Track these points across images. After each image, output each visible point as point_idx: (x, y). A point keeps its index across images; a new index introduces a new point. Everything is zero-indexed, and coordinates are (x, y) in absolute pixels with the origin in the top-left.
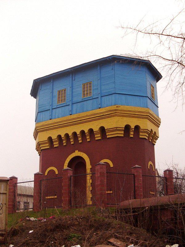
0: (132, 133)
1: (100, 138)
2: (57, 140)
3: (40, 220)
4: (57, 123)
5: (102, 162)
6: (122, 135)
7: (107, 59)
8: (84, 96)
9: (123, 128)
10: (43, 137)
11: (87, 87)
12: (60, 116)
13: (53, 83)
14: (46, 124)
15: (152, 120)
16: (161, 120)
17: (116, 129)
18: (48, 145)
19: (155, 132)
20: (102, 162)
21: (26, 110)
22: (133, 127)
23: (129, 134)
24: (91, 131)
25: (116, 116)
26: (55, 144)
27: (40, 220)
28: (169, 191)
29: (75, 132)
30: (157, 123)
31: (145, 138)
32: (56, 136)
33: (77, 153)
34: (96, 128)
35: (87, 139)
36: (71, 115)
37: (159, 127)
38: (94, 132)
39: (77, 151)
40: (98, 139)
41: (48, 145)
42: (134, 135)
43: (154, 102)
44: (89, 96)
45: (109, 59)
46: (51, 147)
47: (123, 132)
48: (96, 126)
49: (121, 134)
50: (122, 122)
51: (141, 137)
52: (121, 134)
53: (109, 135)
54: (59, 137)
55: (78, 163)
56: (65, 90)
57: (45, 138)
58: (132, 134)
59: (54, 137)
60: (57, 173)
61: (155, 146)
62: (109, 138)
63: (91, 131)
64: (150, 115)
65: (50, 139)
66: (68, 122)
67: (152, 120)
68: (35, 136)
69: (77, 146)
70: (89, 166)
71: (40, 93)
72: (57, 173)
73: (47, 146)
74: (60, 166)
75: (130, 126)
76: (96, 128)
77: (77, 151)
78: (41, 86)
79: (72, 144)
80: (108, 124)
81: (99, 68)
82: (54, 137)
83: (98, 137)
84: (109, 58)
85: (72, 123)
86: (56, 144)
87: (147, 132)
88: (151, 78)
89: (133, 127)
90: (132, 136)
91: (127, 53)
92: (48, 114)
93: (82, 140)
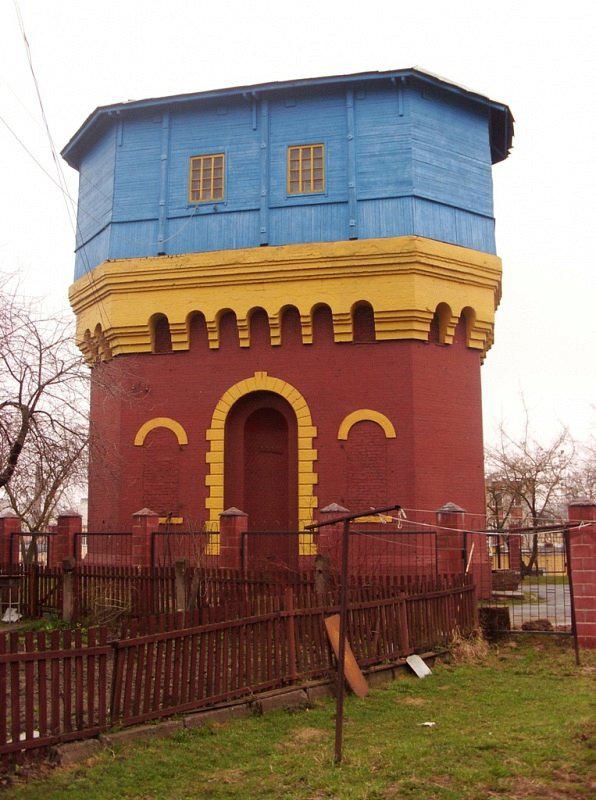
0: (451, 332)
1: (185, 347)
2: (184, 327)
6: (425, 337)
7: (106, 114)
8: (195, 194)
10: (132, 312)
11: (208, 173)
13: (170, 127)
14: (296, 256)
17: (408, 317)
19: (467, 313)
22: (305, 310)
24: (322, 311)
25: (109, 293)
26: (243, 339)
30: (500, 273)
31: (120, 355)
34: (341, 305)
36: (356, 239)
38: (373, 313)
41: (148, 340)
44: (311, 190)
45: (249, 94)
46: (155, 349)
47: (427, 328)
48: (340, 299)
51: (337, 339)
52: (146, 345)
53: (383, 332)
54: (196, 319)
55: (262, 419)
59: (177, 316)
62: (275, 346)
63: (322, 311)
65: (160, 323)
69: (260, 357)
70: (306, 431)
71: (106, 159)
74: (198, 425)
76: (341, 305)
78: (269, 124)
79: (211, 347)
80: (384, 296)
81: (350, 103)
82: (177, 316)
83: (344, 333)
84: (114, 109)
85: (198, 281)
86: (180, 342)
91: (424, 67)
92: (147, 234)
93: (221, 340)
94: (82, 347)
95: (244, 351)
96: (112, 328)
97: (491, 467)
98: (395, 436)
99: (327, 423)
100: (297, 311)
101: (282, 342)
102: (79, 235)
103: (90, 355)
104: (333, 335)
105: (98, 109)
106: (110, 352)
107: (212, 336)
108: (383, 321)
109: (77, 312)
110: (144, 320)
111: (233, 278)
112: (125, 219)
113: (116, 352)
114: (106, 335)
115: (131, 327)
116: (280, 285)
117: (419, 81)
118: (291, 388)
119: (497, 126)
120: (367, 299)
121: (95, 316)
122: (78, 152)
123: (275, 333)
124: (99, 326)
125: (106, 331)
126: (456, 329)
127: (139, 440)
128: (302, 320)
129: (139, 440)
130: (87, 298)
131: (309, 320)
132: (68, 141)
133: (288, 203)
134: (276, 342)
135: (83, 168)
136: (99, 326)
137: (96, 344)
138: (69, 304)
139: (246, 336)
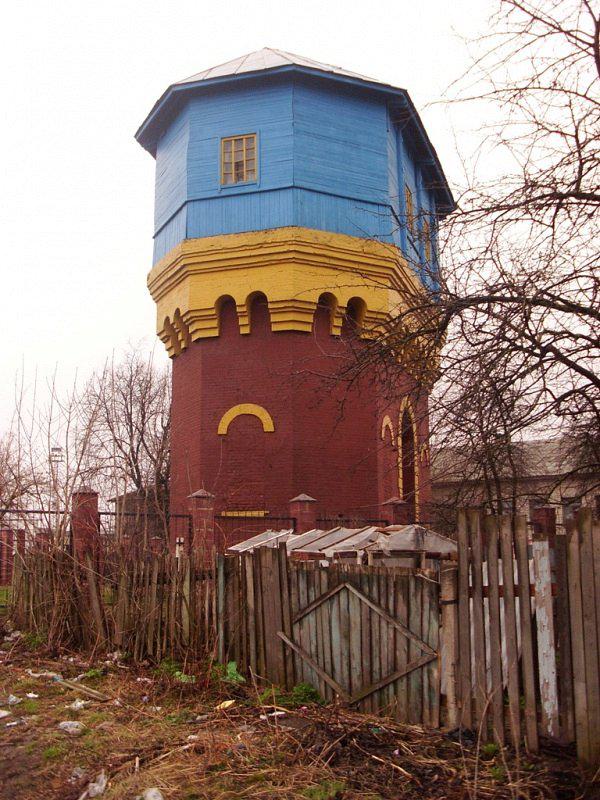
0: (338, 322)
2: (214, 312)
3: (163, 579)
6: (215, 333)
9: (310, 303)
15: (178, 276)
18: (215, 323)
21: (136, 186)
22: (240, 299)
23: (329, 325)
26: (243, 325)
27: (163, 579)
29: (229, 296)
31: (199, 339)
32: (215, 300)
40: (300, 329)
42: (343, 329)
47: (310, 319)
49: (305, 323)
51: (275, 328)
52: (305, 323)
53: (280, 322)
56: (250, 139)
58: (338, 327)
60: (269, 426)
62: (275, 332)
64: (396, 269)
67: (178, 276)
68: (161, 286)
72: (269, 426)
73: (209, 329)
75: (363, 301)
79: (242, 332)
88: (180, 125)
89: (343, 301)
93: (253, 324)
94: (163, 336)
95: (246, 338)
96: (189, 312)
98: (273, 430)
100: (266, 297)
101: (251, 330)
102: (156, 222)
104: (269, 324)
105: (171, 87)
106: (189, 336)
107: (242, 321)
109: (157, 300)
112: (209, 196)
113: (195, 338)
114: (184, 320)
115: (306, 302)
116: (229, 273)
117: (220, 85)
120: (256, 288)
121: (183, 299)
122: (153, 135)
124: (178, 311)
125: (184, 315)
126: (344, 320)
127: (222, 429)
128: (238, 310)
129: (222, 429)
130: (173, 276)
133: (224, 193)
134: (245, 331)
135: (158, 155)
136: (178, 311)
137: (173, 330)
138: (148, 292)
139: (215, 325)
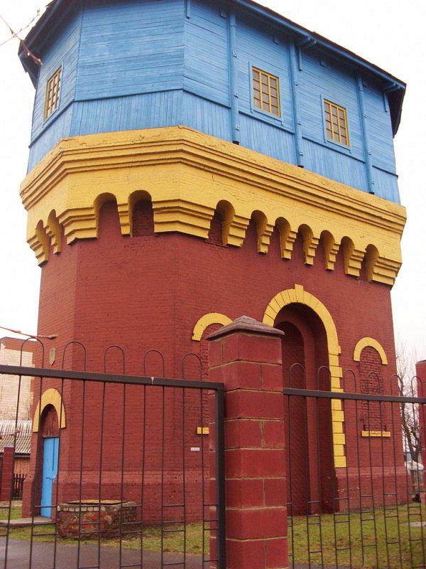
0: (125, 220)
1: (238, 243)
2: (93, 212)
4: (264, 169)
5: (198, 333)
10: (78, 194)
12: (104, 132)
15: (44, 187)
16: (407, 211)
17: (192, 210)
20: (198, 333)
22: (123, 198)
28: (214, 508)
30: (394, 223)
33: (298, 295)
35: (119, 226)
37: (400, 233)
39: (299, 288)
43: (348, 153)
47: (207, 225)
50: (206, 191)
52: (201, 229)
53: (162, 224)
57: (88, 200)
61: (393, 292)
65: (223, 212)
66: (93, 156)
69: (295, 271)
77: (299, 288)
80: (163, 185)
86: (235, 237)
87: (71, 217)
89: (123, 198)
90: (264, 249)
96: (179, 200)
97: (34, 366)
99: (347, 345)
103: (40, 251)
108: (161, 211)
110: (89, 201)
111: (89, 164)
113: (70, 240)
118: (273, 301)
119: (390, 92)
123: (125, 220)
124: (53, 212)
126: (212, 222)
131: (127, 208)
132: (312, 30)
